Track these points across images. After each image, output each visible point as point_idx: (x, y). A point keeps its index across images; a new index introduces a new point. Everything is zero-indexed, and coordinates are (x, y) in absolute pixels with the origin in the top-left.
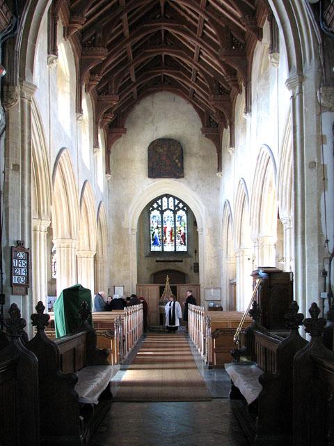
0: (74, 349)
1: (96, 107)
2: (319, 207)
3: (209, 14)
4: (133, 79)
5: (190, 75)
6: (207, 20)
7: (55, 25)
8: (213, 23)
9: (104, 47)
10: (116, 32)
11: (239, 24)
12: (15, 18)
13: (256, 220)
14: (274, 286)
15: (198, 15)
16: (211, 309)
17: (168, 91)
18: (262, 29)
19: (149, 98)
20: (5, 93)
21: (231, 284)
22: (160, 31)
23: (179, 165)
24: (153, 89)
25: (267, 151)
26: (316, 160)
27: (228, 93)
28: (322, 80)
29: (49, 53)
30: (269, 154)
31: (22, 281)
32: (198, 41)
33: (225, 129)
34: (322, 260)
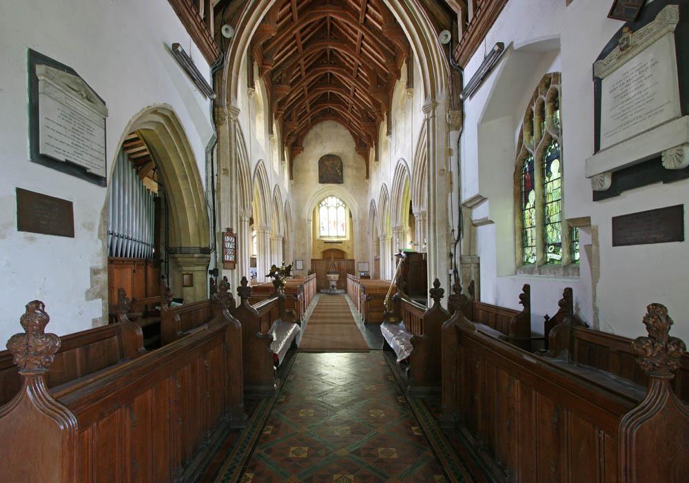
0: (270, 312)
1: (283, 130)
2: (447, 204)
3: (362, 60)
4: (308, 111)
5: (347, 108)
6: (360, 64)
7: (253, 65)
8: (367, 70)
9: (287, 84)
10: (296, 73)
11: (382, 67)
12: (222, 53)
13: (394, 214)
14: (413, 266)
15: (353, 61)
16: (362, 277)
17: (332, 120)
18: (400, 71)
19: (319, 125)
20: (216, 114)
21: (376, 260)
22: (326, 74)
23: (340, 174)
24: (322, 118)
25: (403, 163)
26: (445, 168)
27: (374, 121)
28: (450, 105)
29: (248, 87)
30: (405, 165)
31: (231, 258)
32: (353, 81)
33: (371, 149)
34: (449, 245)
